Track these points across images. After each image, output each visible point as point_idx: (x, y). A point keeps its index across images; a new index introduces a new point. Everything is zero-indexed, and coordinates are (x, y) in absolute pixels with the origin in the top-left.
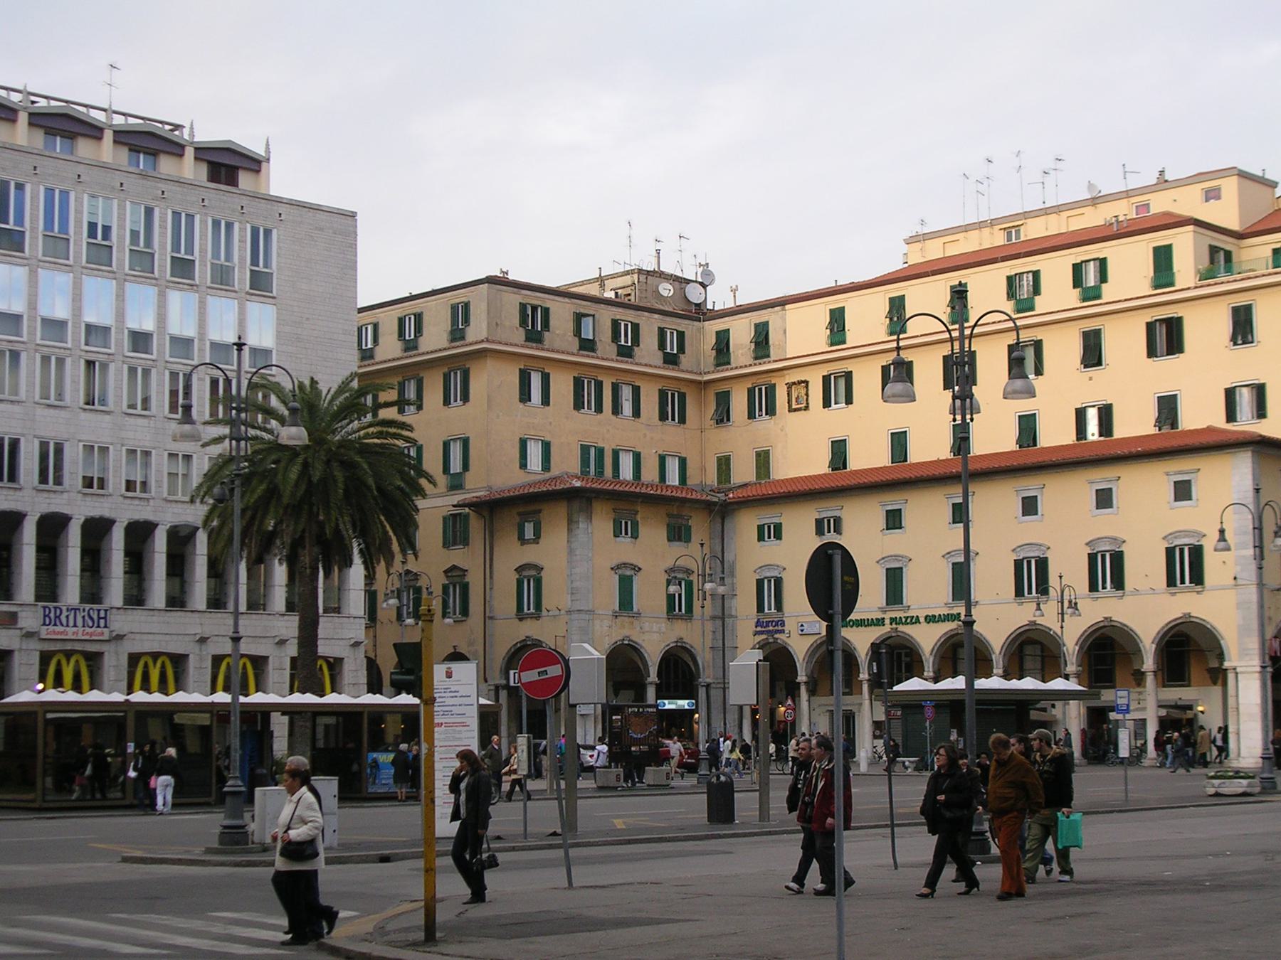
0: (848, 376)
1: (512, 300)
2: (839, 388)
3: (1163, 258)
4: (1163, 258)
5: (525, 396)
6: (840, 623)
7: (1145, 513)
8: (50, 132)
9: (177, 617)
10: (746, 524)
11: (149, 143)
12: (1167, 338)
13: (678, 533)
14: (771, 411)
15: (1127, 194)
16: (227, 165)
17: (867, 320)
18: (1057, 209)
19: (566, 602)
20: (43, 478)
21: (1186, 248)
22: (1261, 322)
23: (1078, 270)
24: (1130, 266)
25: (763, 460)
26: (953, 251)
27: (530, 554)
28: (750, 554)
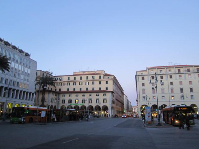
0: (76, 83)
1: (42, 72)
2: (68, 83)
3: (100, 77)
4: (100, 77)
5: (92, 84)
6: (166, 108)
7: (101, 96)
8: (13, 48)
9: (19, 100)
10: (61, 95)
11: (21, 51)
12: (93, 83)
13: (56, 95)
14: (61, 85)
15: (94, 71)
16: (27, 55)
17: (72, 78)
18: (88, 71)
19: (48, 101)
20: (13, 85)
21: (102, 76)
22: (101, 83)
23: (92, 77)
24: (97, 77)
25: (60, 89)
26: (78, 74)
27: (64, 98)
28: (61, 97)
